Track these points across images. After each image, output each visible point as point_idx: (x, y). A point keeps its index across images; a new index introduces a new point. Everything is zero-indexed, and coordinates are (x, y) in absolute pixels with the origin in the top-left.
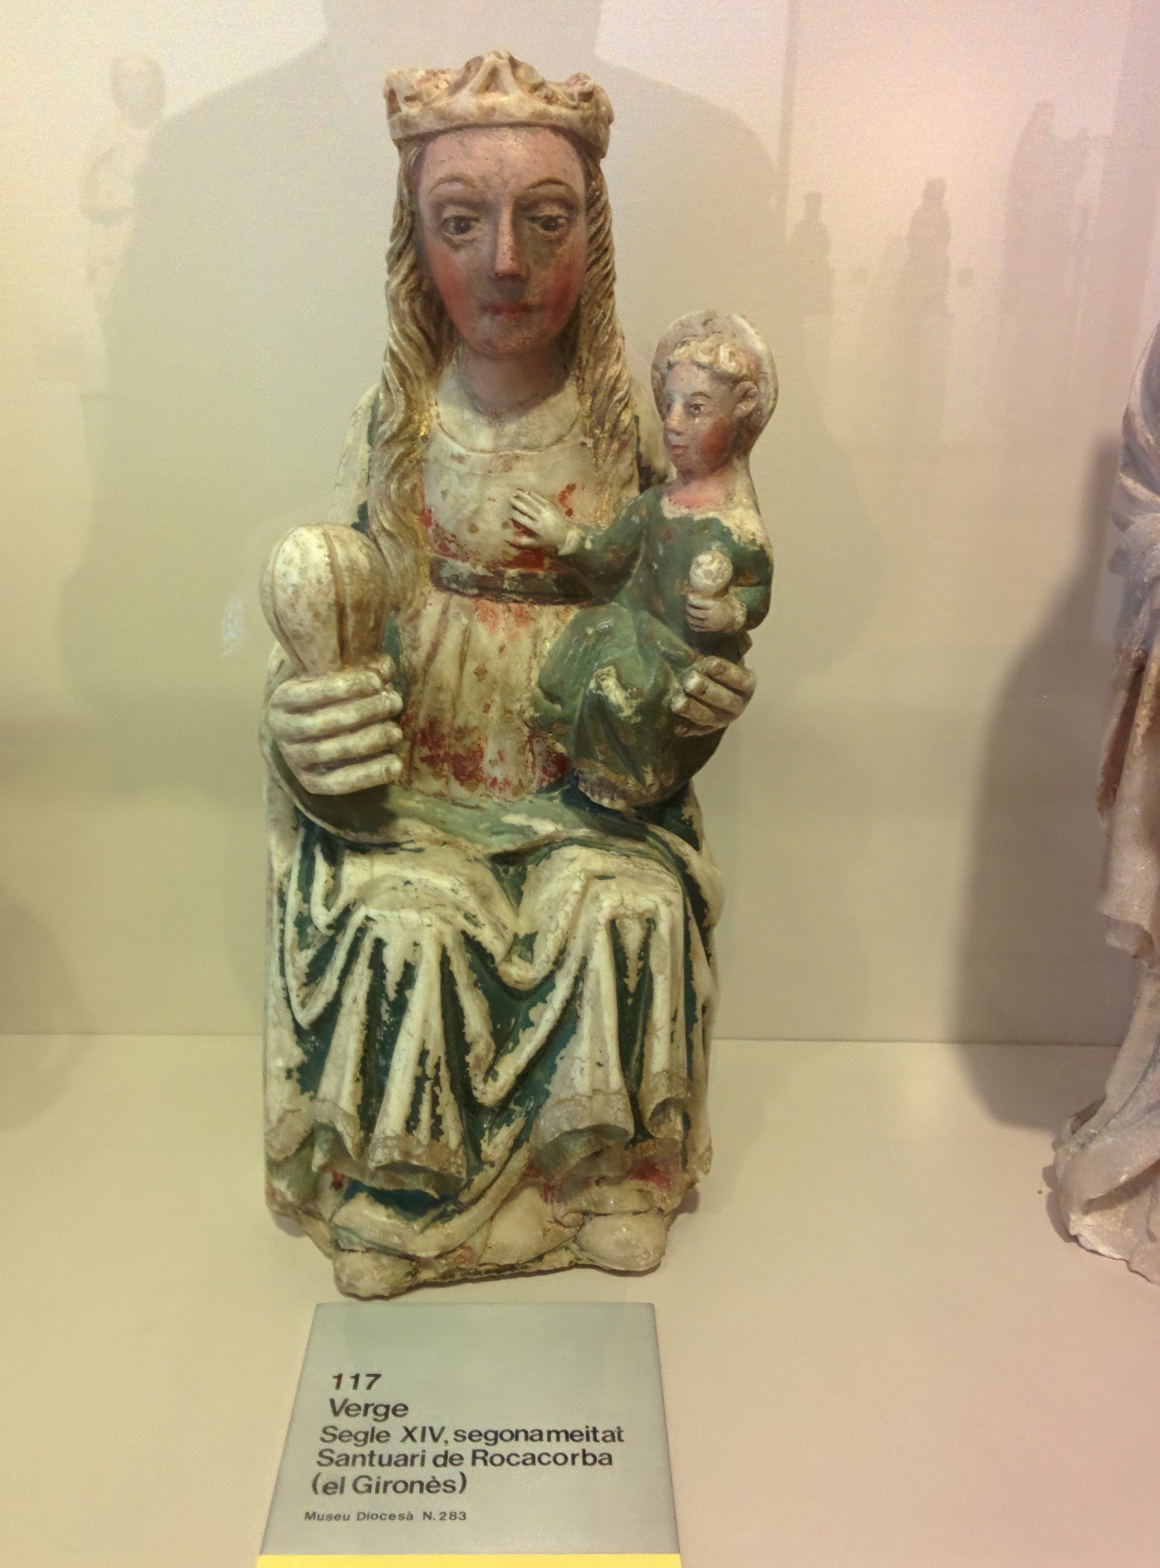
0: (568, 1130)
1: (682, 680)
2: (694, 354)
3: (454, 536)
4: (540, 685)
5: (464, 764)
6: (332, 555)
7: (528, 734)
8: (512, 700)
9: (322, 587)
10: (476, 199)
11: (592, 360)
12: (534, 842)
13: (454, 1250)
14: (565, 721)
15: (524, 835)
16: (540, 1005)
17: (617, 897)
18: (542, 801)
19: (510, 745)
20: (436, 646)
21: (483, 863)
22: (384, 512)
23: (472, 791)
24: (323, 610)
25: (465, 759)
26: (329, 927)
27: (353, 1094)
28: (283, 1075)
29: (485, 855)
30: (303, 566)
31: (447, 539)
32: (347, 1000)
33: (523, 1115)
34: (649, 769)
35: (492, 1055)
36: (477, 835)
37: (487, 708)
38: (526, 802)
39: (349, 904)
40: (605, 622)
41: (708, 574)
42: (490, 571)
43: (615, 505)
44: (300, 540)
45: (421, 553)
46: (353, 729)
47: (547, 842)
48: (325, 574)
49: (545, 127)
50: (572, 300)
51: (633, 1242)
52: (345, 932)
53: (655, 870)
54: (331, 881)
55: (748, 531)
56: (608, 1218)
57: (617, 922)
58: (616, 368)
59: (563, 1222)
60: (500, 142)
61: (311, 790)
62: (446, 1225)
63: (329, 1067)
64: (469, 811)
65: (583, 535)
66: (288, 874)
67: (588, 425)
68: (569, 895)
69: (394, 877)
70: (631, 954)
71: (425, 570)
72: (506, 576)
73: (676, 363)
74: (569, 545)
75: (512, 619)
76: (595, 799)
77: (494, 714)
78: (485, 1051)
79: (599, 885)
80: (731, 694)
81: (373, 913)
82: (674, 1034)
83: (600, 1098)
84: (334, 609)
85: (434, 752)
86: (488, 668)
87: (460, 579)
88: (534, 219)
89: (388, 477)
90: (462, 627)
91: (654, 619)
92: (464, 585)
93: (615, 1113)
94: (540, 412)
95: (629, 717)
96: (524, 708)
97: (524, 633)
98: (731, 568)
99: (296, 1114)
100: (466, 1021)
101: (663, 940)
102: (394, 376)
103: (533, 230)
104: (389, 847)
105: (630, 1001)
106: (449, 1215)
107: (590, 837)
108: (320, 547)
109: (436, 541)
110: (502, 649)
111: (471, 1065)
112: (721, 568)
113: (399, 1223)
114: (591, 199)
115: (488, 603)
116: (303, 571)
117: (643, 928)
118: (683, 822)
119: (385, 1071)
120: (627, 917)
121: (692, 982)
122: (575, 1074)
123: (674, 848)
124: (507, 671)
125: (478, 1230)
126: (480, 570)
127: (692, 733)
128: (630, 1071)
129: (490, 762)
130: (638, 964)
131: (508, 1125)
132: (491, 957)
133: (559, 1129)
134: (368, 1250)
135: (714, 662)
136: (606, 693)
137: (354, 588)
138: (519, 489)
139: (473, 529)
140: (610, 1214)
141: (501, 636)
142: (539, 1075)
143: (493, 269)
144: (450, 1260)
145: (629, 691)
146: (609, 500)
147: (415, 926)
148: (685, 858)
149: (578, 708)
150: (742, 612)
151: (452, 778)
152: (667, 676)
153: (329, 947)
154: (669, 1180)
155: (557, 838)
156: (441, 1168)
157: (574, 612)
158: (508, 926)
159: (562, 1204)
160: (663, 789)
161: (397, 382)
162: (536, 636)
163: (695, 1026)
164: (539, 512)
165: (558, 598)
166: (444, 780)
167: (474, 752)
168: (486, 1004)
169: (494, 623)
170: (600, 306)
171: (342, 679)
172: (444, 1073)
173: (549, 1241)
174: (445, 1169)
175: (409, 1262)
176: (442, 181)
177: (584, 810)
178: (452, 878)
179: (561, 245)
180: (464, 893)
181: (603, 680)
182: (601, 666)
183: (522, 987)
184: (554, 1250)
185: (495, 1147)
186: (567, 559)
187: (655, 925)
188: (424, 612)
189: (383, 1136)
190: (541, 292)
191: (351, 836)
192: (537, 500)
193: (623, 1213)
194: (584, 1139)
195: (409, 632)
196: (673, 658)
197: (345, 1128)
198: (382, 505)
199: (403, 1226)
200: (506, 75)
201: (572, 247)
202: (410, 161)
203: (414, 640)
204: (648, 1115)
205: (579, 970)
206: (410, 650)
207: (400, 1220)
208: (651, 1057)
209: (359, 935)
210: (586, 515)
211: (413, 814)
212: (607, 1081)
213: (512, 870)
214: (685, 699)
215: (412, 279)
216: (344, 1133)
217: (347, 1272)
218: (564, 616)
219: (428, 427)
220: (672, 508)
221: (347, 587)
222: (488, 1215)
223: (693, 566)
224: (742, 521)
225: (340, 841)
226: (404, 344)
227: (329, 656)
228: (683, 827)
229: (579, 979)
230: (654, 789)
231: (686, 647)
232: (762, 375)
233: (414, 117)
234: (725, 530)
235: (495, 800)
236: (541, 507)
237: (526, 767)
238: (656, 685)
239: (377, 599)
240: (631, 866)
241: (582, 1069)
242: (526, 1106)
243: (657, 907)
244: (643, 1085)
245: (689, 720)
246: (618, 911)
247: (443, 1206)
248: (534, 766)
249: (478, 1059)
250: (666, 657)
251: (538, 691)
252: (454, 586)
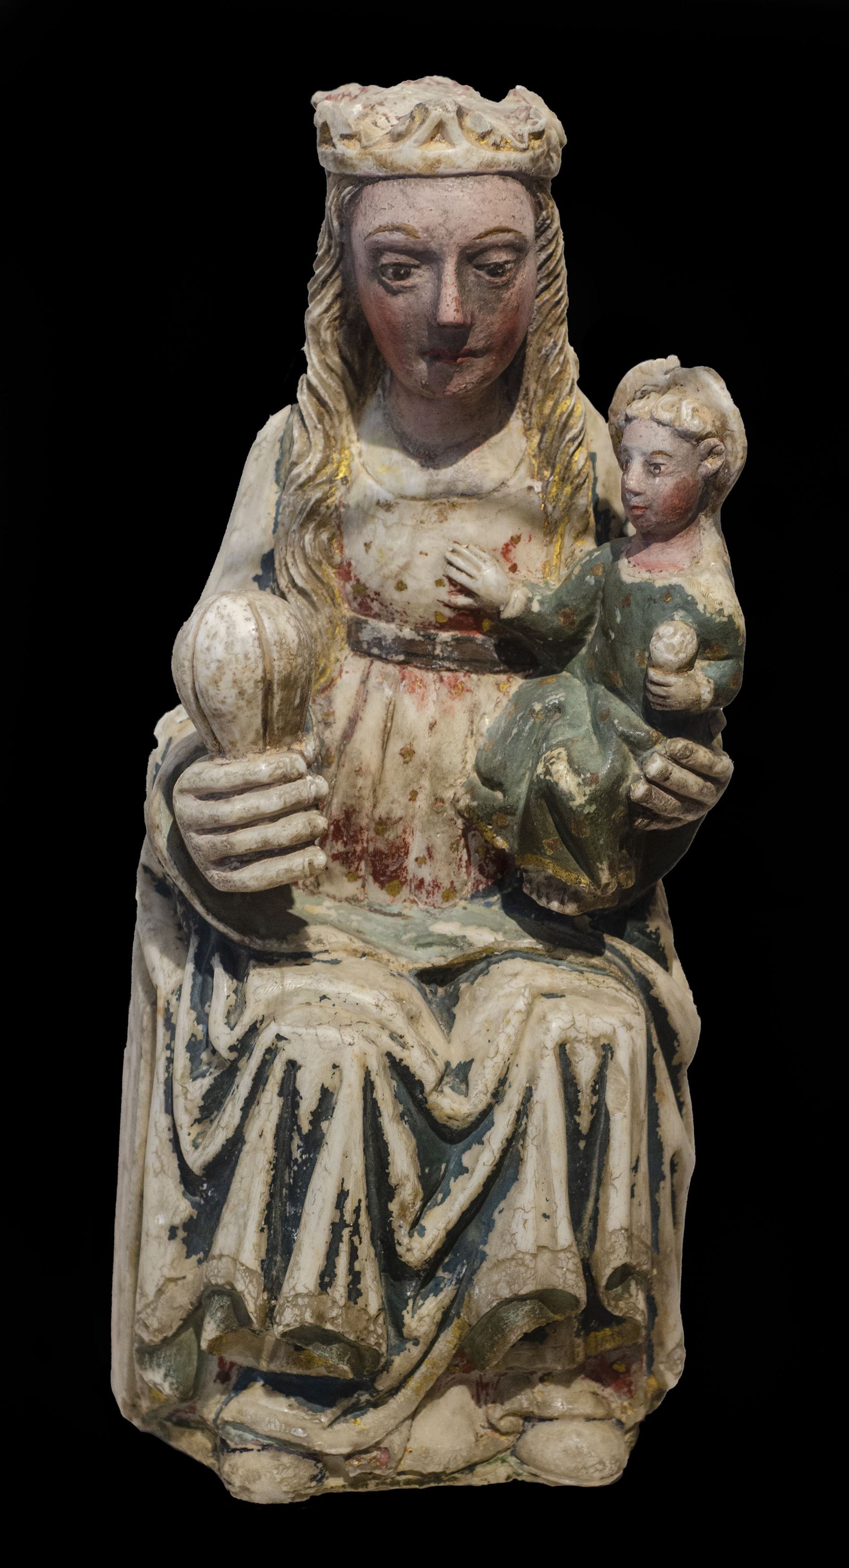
0: (508, 1296)
1: (642, 765)
2: (654, 410)
3: (377, 594)
4: (477, 769)
5: (385, 862)
6: (259, 628)
7: (461, 827)
8: (444, 787)
9: (249, 662)
10: (420, 248)
11: (540, 392)
12: (469, 955)
13: (366, 1451)
14: (506, 810)
15: (457, 947)
16: (476, 1147)
17: (568, 1018)
18: (477, 907)
19: (441, 839)
20: (354, 721)
21: (408, 980)
22: (297, 566)
23: (394, 896)
24: (249, 687)
25: (387, 856)
26: (232, 1048)
27: (258, 1245)
28: (165, 1235)
29: (410, 971)
30: (230, 640)
31: (369, 596)
32: (251, 1135)
33: (454, 1283)
34: (605, 866)
35: (419, 1204)
36: (401, 948)
37: (414, 796)
38: (459, 908)
39: (256, 1022)
40: (554, 697)
41: (670, 648)
42: (419, 635)
43: (566, 560)
44: (225, 612)
45: (337, 613)
46: (274, 817)
47: (484, 955)
48: (254, 651)
49: (494, 174)
50: (519, 339)
51: (585, 1450)
52: (251, 1054)
53: (613, 988)
54: (233, 996)
55: (714, 600)
56: (555, 1423)
57: (568, 1047)
58: (568, 402)
59: (498, 1427)
60: (446, 194)
61: (220, 888)
62: (358, 1420)
63: (227, 1216)
64: (390, 920)
65: (530, 595)
66: (178, 992)
67: (536, 466)
68: (511, 1013)
69: (307, 990)
70: (584, 1086)
71: (341, 632)
72: (438, 640)
73: (635, 418)
74: (513, 607)
75: (444, 690)
76: (543, 902)
77: (422, 802)
78: (411, 1197)
79: (545, 1004)
80: (700, 781)
81: (285, 1031)
82: (635, 1188)
83: (546, 1256)
84: (261, 685)
85: (349, 848)
86: (415, 748)
87: (383, 643)
88: (479, 267)
89: (302, 526)
90: (384, 700)
91: (610, 694)
92: (388, 650)
93: (564, 1274)
94: (479, 454)
95: (582, 806)
96: (458, 796)
97: (460, 708)
98: (695, 642)
99: (180, 1282)
100: (390, 1159)
101: (621, 1072)
102: (312, 412)
103: (478, 276)
104: (301, 957)
105: (582, 1144)
106: (361, 1409)
107: (536, 949)
108: (247, 619)
109: (355, 598)
110: (432, 726)
111: (394, 1215)
112: (683, 641)
113: (303, 1414)
114: (541, 227)
115: (417, 672)
116: (229, 646)
117: (598, 1055)
118: (648, 936)
119: (295, 1221)
120: (580, 1041)
121: (658, 1129)
122: (517, 1227)
123: (637, 964)
124: (437, 752)
125: (397, 1428)
126: (407, 633)
127: (654, 826)
128: (582, 1232)
129: (416, 860)
130: (591, 1098)
131: (436, 1295)
132: (420, 1084)
133: (497, 1295)
134: (264, 1447)
135: (680, 744)
136: (555, 778)
137: (282, 663)
138: (455, 542)
139: (401, 586)
140: (557, 1419)
141: (431, 711)
142: (472, 1233)
143: (435, 319)
144: (363, 1462)
145: (582, 776)
146: (560, 553)
147: (334, 1044)
148: (649, 977)
149: (523, 796)
150: (709, 689)
151: (370, 879)
152: (625, 759)
153: (230, 1072)
154: (630, 1384)
155: (496, 951)
156: (358, 1338)
157: (517, 683)
158: (438, 1052)
159: (498, 1405)
160: (622, 893)
161: (315, 419)
162: (474, 710)
163: (662, 1184)
164: (479, 569)
165: (499, 666)
166: (359, 882)
167: (398, 848)
168: (414, 1141)
169: (423, 696)
170: (550, 335)
171: (265, 761)
172: (364, 1220)
173: (481, 1448)
174: (362, 1340)
175: (314, 1462)
176: (382, 229)
177: (529, 917)
178: (376, 992)
179: (508, 289)
180: (390, 1009)
181: (552, 764)
182: (550, 748)
183: (454, 1125)
184: (486, 1461)
185: (421, 1319)
186: (510, 622)
187: (612, 1053)
188: (339, 682)
189: (292, 1293)
190: (485, 337)
191: (257, 944)
192: (476, 555)
193: (573, 1417)
194: (527, 1308)
195: (321, 705)
196: (632, 739)
197: (247, 1287)
198: (294, 557)
199: (307, 1417)
200: (453, 127)
201: (520, 289)
202: (344, 198)
203: (328, 715)
204: (604, 1282)
205: (523, 1104)
206: (321, 726)
207: (304, 1411)
208: (607, 1212)
209: (267, 1057)
210: (533, 571)
211: (324, 922)
212: (554, 1236)
213: (441, 991)
214: (646, 786)
215: (336, 307)
216: (246, 1293)
217: (240, 1472)
218: (506, 687)
219: (349, 466)
220: (631, 570)
221: (276, 663)
222: (409, 1412)
223: (654, 638)
224: (708, 589)
225: (242, 951)
226: (325, 376)
227: (251, 736)
228: (647, 940)
229: (523, 1113)
230: (611, 889)
231: (647, 727)
232: (729, 432)
233: (351, 159)
234: (690, 598)
235: (421, 906)
236: (480, 563)
237: (460, 866)
238: (612, 769)
239: (304, 674)
240: (585, 983)
241: (526, 1221)
242: (457, 1272)
243: (614, 1031)
244: (597, 1247)
245: (650, 810)
246: (568, 1035)
247: (356, 1395)
248: (469, 862)
249: (403, 1208)
250: (625, 738)
251: (474, 775)
252: (375, 651)
